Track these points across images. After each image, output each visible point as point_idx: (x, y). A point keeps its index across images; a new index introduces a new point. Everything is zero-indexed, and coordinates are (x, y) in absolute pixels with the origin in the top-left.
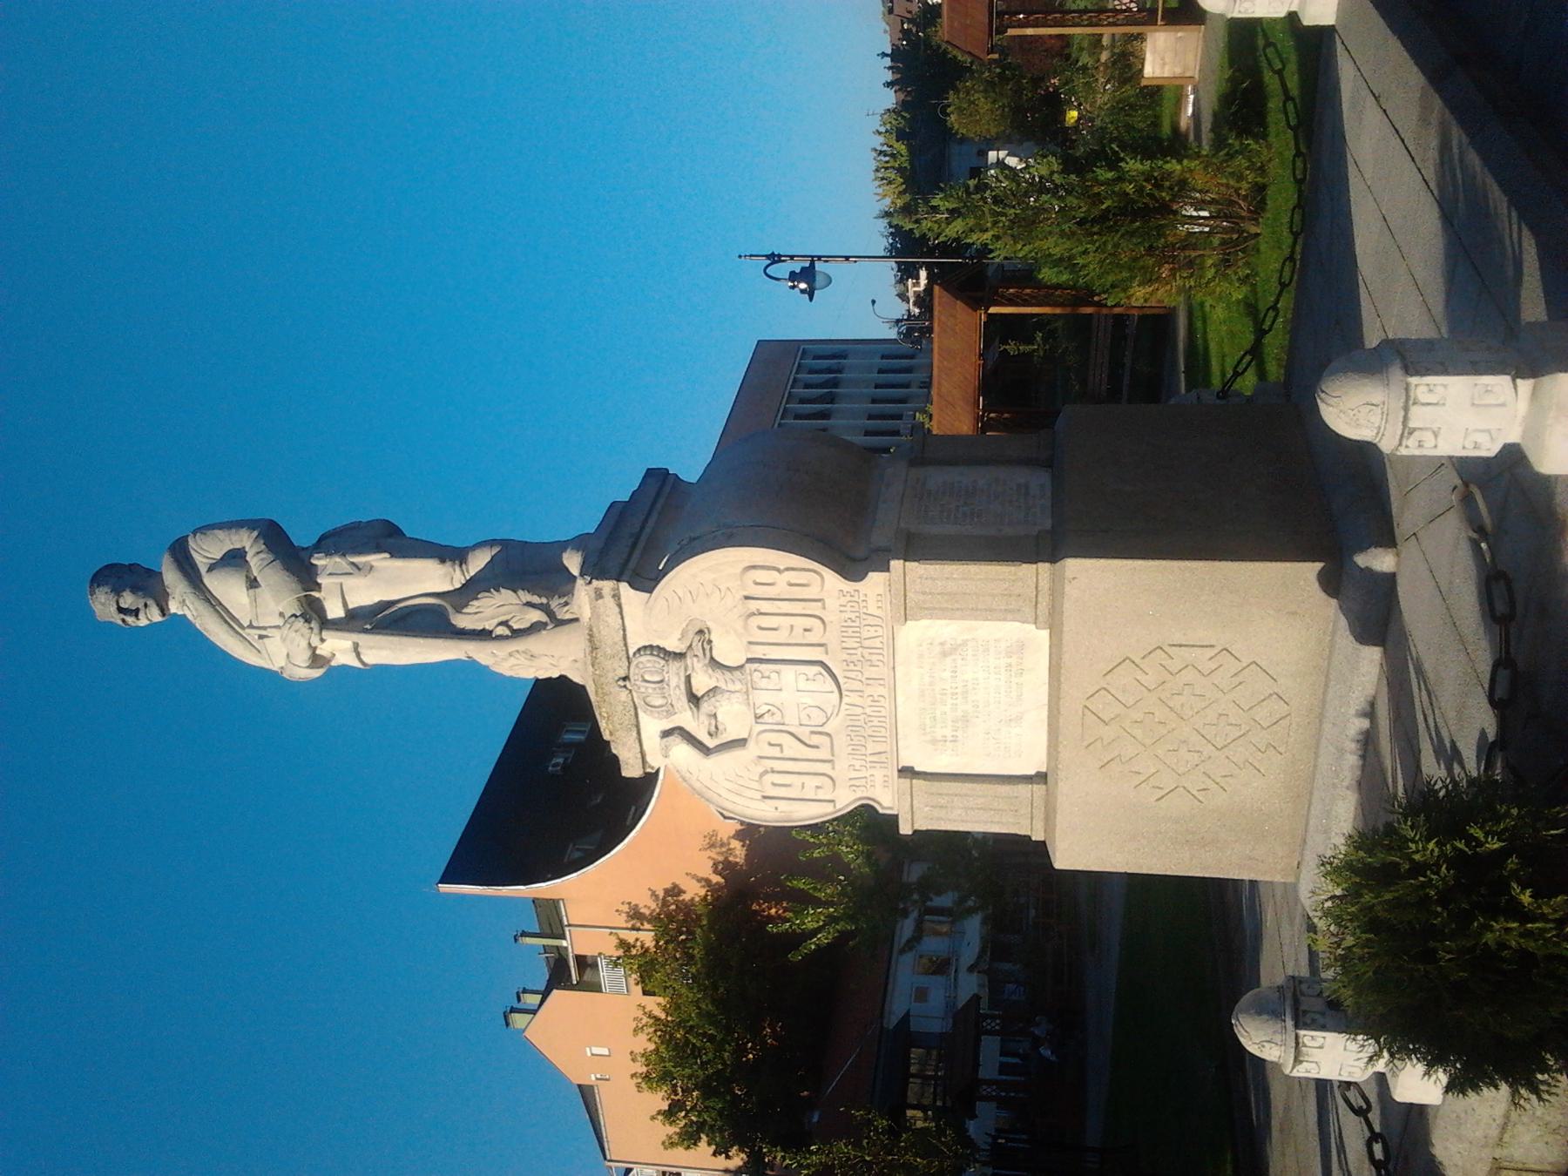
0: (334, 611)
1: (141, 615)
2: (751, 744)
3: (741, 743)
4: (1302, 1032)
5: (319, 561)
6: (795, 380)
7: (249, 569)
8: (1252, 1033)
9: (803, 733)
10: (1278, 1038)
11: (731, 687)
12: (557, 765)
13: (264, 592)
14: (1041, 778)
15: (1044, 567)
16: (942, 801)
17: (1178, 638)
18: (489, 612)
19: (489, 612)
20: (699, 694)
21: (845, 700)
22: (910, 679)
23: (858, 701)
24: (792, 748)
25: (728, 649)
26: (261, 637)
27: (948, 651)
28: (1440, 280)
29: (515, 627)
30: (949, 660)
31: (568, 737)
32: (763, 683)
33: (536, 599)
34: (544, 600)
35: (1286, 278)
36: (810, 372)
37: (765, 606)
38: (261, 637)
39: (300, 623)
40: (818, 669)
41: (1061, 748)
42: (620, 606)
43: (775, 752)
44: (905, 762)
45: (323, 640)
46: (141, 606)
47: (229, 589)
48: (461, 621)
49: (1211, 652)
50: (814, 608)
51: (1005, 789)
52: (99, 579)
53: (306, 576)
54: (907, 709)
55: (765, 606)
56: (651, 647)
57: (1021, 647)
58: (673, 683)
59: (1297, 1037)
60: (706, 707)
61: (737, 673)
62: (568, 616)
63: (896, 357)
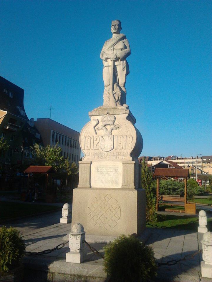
0: (116, 63)
1: (114, 29)
2: (96, 135)
3: (96, 133)
4: (80, 236)
5: (125, 61)
6: (74, 140)
7: (124, 49)
8: (78, 227)
9: (99, 144)
10: (78, 231)
11: (108, 132)
12: (5, 91)
13: (121, 52)
14: (91, 187)
15: (134, 187)
16: (86, 169)
17: (122, 210)
18: (117, 90)
19: (117, 90)
20: (106, 127)
21: (106, 152)
22: (110, 164)
23: (106, 155)
24: (96, 143)
25: (115, 132)
26: (112, 50)
27: (116, 171)
28: (192, 250)
29: (115, 95)
30: (114, 170)
31: (10, 94)
32: (109, 138)
33: (119, 99)
34: (119, 100)
35: (154, 226)
36: (76, 143)
37: (125, 139)
38: (112, 50)
39: (115, 57)
40: (113, 148)
41: (99, 190)
42: (124, 114)
43: (95, 139)
44: (93, 163)
45: (111, 61)
46: (116, 29)
47: (120, 45)
48: (115, 85)
49: (119, 216)
50: (124, 147)
51: (88, 180)
52: (120, 22)
53: (124, 59)
54: (103, 163)
55: (125, 139)
56: (115, 119)
57: (117, 183)
58: (109, 122)
59: (79, 235)
60: (104, 127)
61: (110, 134)
62: (117, 104)
63: (77, 158)
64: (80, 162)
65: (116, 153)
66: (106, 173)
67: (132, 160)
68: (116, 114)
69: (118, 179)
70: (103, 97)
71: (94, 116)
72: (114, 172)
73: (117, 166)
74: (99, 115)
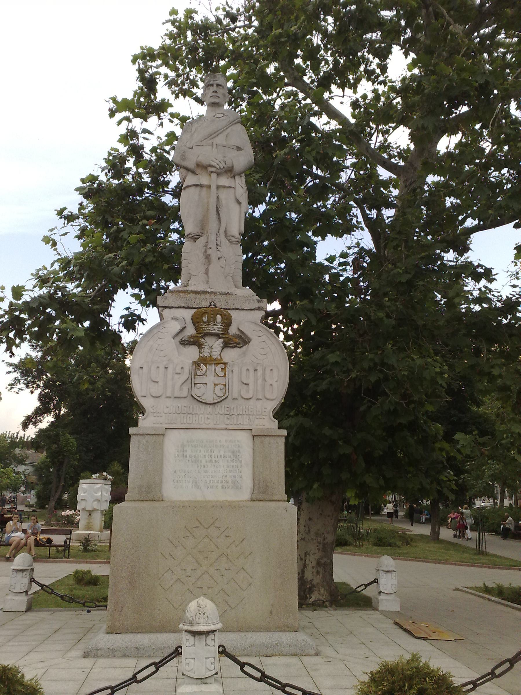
27: (235, 455)
30: (230, 454)
57: (236, 486)
64: (132, 430)
65: (237, 407)
66: (209, 461)
67: (279, 429)
68: (234, 309)
69: (241, 477)
70: (125, 328)
71: (172, 307)
72: (229, 459)
73: (238, 441)
74: (187, 308)
